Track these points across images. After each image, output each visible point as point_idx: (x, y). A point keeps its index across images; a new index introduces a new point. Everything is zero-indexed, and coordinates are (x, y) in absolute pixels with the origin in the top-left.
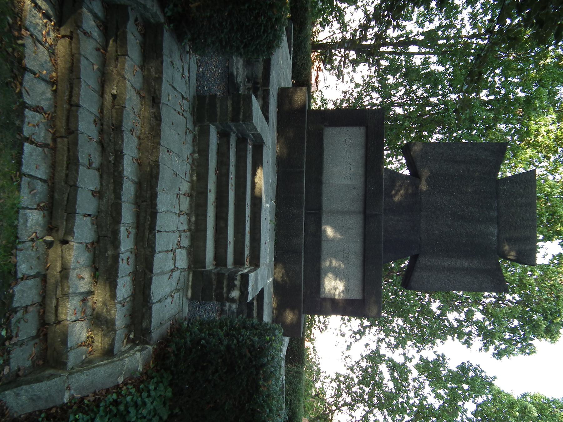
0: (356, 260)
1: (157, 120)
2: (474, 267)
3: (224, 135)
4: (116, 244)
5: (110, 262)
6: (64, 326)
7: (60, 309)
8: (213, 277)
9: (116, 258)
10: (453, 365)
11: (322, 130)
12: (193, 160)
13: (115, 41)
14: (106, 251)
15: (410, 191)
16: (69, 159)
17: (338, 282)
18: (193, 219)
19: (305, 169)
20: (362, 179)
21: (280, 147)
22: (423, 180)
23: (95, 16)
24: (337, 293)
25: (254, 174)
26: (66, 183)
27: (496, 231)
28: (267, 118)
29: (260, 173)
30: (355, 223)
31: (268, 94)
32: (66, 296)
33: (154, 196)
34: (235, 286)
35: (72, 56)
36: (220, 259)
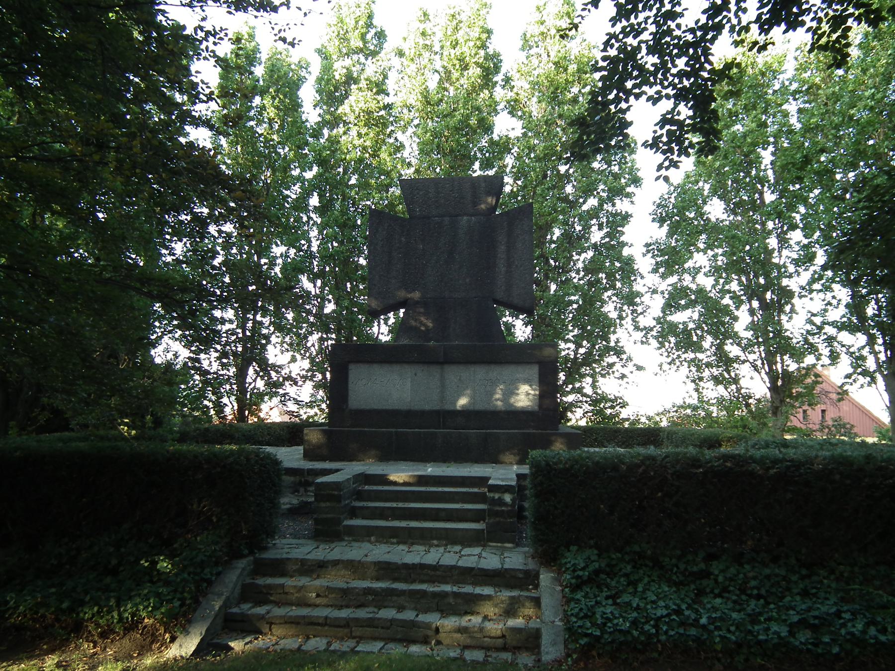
0: (495, 372)
1: (338, 564)
2: (505, 240)
3: (354, 513)
4: (444, 595)
5: (460, 601)
6: (506, 631)
7: (492, 635)
8: (492, 521)
9: (456, 595)
10: (660, 233)
11: (351, 410)
12: (377, 541)
13: (271, 595)
14: (450, 604)
15: (422, 310)
16: (369, 626)
17: (520, 391)
18: (435, 542)
19: (394, 430)
20: (406, 366)
21: (369, 458)
22: (409, 296)
23: (253, 607)
24: (532, 392)
25: (395, 483)
26: (388, 628)
27: (465, 218)
28: (337, 470)
29: (393, 477)
30: (454, 373)
31: (312, 470)
32: (481, 629)
33: (406, 566)
34: (499, 498)
35: (286, 623)
36: (477, 516)
